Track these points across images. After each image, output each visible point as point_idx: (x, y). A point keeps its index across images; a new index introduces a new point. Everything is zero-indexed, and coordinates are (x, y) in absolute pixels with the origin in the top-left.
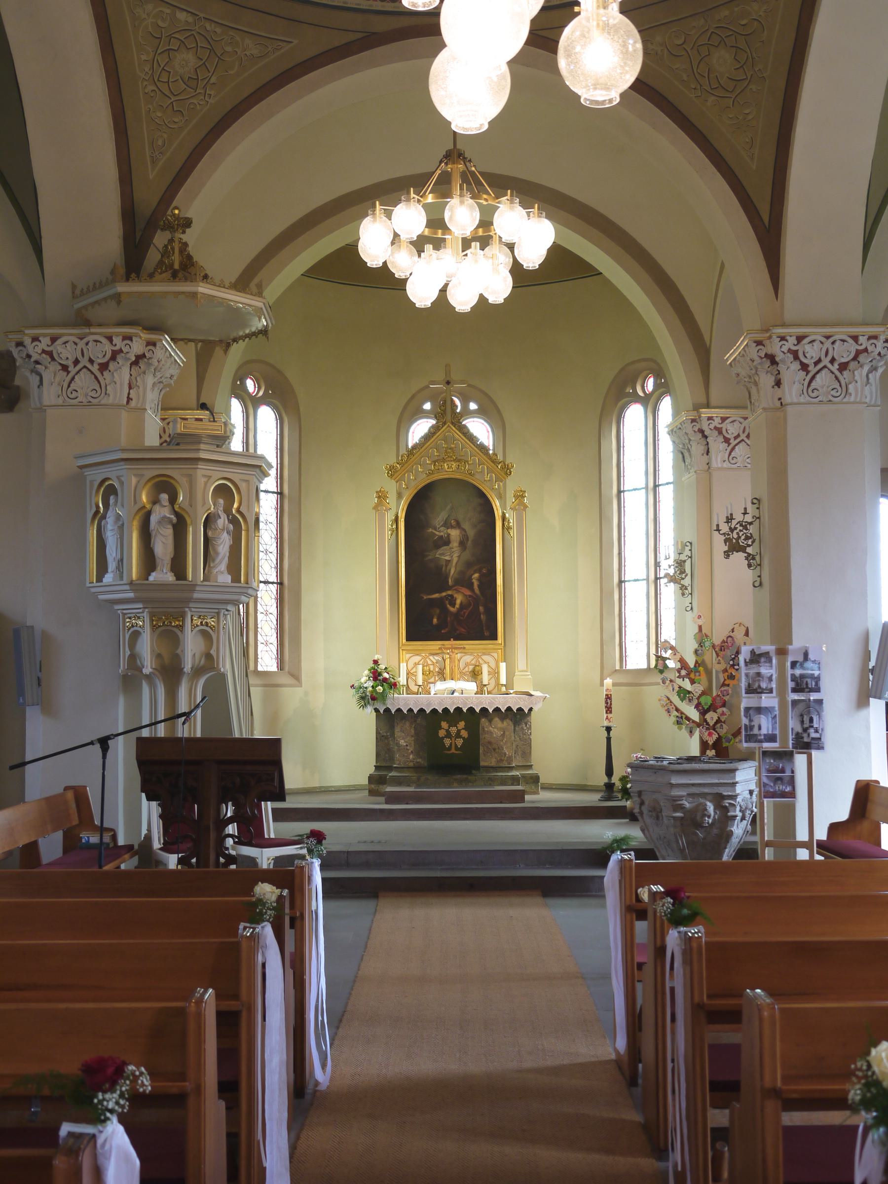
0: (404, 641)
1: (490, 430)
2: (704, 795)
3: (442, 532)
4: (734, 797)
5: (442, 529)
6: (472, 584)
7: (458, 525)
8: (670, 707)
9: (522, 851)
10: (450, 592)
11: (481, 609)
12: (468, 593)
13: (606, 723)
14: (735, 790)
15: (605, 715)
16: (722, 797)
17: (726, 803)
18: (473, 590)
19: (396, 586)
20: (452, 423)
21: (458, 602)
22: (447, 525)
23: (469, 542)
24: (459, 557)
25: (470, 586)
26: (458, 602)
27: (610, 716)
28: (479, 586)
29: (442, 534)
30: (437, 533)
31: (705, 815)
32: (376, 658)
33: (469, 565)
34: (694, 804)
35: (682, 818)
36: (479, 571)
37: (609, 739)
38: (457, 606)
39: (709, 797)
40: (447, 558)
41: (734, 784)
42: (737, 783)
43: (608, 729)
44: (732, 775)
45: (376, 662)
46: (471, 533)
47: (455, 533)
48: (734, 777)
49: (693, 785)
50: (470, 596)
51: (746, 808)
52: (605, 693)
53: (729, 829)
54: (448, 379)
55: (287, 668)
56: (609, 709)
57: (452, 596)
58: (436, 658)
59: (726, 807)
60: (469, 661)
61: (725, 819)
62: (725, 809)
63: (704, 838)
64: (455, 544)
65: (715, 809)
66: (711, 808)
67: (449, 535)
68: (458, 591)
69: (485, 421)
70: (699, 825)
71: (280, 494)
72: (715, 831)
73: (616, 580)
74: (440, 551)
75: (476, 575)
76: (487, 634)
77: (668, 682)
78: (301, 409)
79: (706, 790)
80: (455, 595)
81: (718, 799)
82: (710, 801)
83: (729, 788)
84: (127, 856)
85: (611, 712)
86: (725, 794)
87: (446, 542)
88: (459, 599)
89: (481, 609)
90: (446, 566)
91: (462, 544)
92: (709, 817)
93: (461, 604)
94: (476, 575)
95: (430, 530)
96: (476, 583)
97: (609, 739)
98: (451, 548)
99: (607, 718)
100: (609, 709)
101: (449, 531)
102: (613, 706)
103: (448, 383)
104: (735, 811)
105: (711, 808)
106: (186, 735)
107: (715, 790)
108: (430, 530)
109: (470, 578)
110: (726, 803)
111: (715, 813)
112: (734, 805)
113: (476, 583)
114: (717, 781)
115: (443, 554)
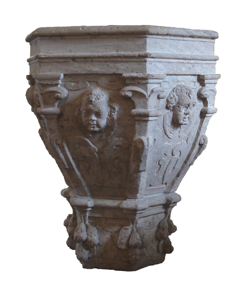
2: (93, 78)
4: (143, 81)
16: (124, 81)
31: (89, 112)
34: (78, 93)
39: (104, 81)
41: (142, 58)
44: (139, 42)
49: (74, 59)
53: (137, 137)
59: (129, 98)
62: (128, 102)
63: (100, 152)
65: (111, 101)
66: (101, 97)
70: (84, 129)
72: (116, 140)
79: (96, 68)
81: (116, 82)
82: (104, 88)
83: (134, 66)
84: (86, 261)
86: (125, 75)
92: (98, 114)
105: (101, 97)
106: (205, 82)
107: (110, 68)
110: (127, 91)
111: (112, 108)
112: (142, 96)
114: (114, 53)
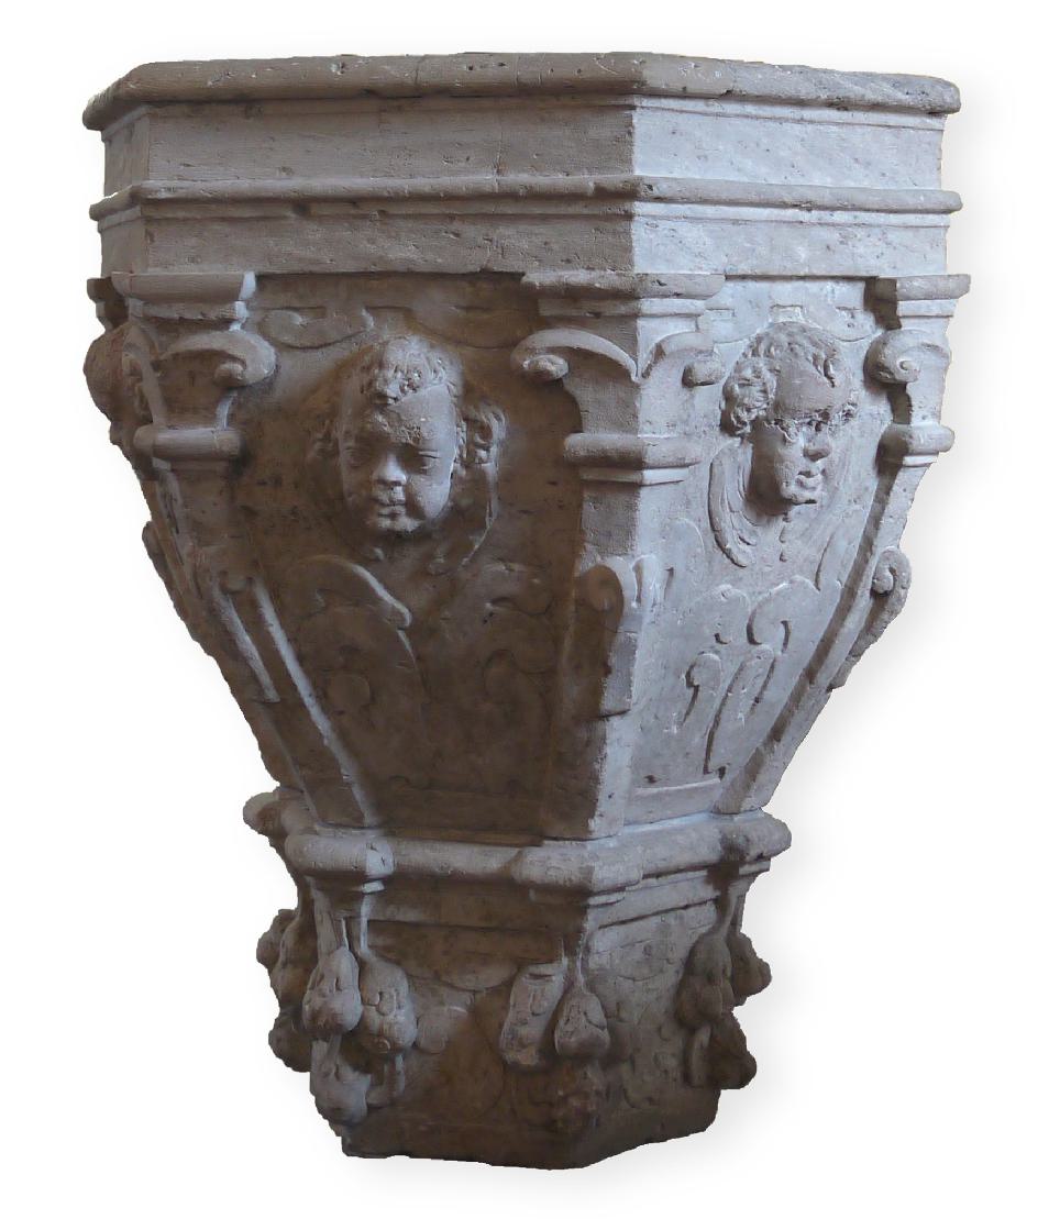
2: (392, 291)
4: (614, 305)
19: (754, 197)
31: (372, 447)
34: (322, 361)
35: (239, 463)
41: (614, 203)
42: (630, 193)
44: (601, 129)
49: (303, 205)
51: (780, 409)
53: (588, 561)
63: (422, 630)
65: (470, 397)
66: (424, 380)
70: (349, 522)
72: (495, 575)
79: (404, 249)
83: (580, 236)
92: (414, 458)
105: (424, 380)
107: (471, 248)
110: (547, 353)
112: (613, 372)
114: (487, 179)
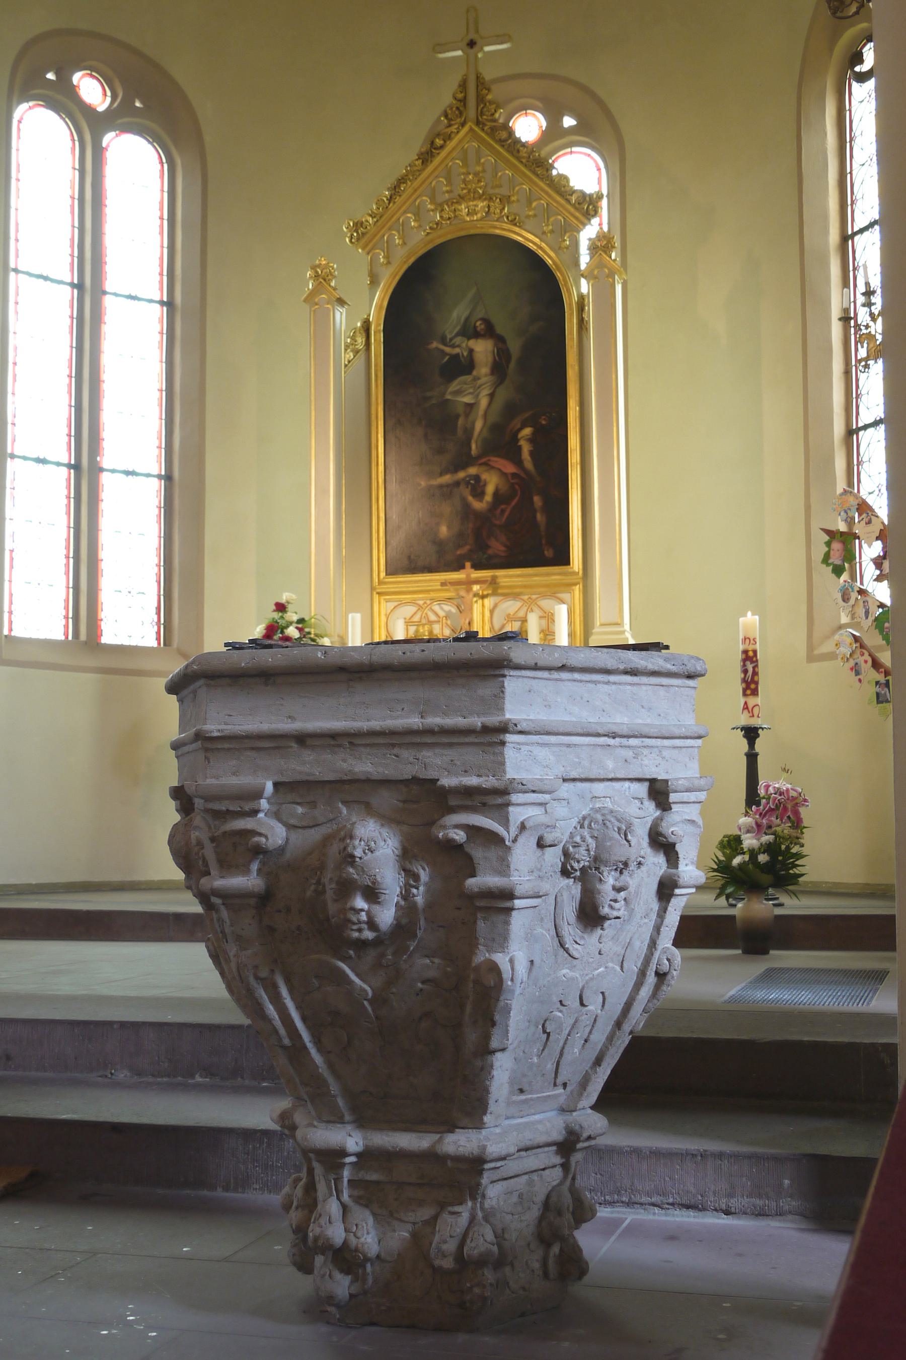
0: (383, 574)
1: (601, 164)
2: (357, 791)
3: (461, 347)
4: (495, 799)
5: (458, 340)
6: (520, 448)
7: (489, 331)
8: (861, 660)
9: (123, 1025)
10: (473, 471)
11: (537, 500)
12: (510, 468)
13: (744, 720)
14: (500, 765)
15: (742, 700)
17: (453, 828)
18: (519, 462)
20: (478, 123)
21: (490, 489)
22: (469, 332)
23: (513, 364)
24: (492, 396)
25: (513, 454)
26: (490, 489)
27: (752, 701)
28: (532, 454)
29: (457, 350)
30: (448, 350)
31: (346, 888)
32: (283, 600)
33: (510, 410)
34: (315, 835)
35: (264, 899)
36: (531, 422)
37: (752, 758)
38: (488, 498)
39: (386, 799)
40: (467, 399)
41: (494, 734)
43: (751, 734)
44: (485, 690)
45: (281, 607)
46: (515, 346)
47: (483, 349)
48: (497, 700)
49: (302, 739)
50: (514, 475)
51: (597, 861)
52: (741, 647)
53: (481, 956)
54: (472, 36)
55: (175, 643)
56: (750, 686)
57: (477, 478)
58: (447, 608)
60: (512, 611)
61: (465, 909)
62: (456, 859)
63: (379, 1000)
64: (483, 370)
65: (406, 856)
66: (378, 847)
67: (471, 351)
68: (488, 466)
69: (593, 148)
70: (334, 934)
71: (169, 304)
72: (424, 966)
73: (839, 428)
74: (454, 386)
75: (527, 431)
76: (549, 553)
77: (854, 595)
78: (207, 139)
79: (365, 765)
80: (485, 476)
81: (421, 806)
82: (388, 819)
83: (471, 756)
85: (755, 692)
86: (447, 781)
87: (462, 366)
88: (492, 483)
89: (537, 500)
90: (467, 415)
91: (499, 369)
92: (372, 894)
93: (496, 494)
94: (527, 431)
95: (435, 345)
96: (526, 448)
97: (752, 758)
98: (477, 379)
99: (746, 707)
100: (750, 686)
101: (472, 343)
102: (761, 678)
103: (472, 44)
104: (504, 868)
105: (378, 847)
108: (435, 345)
109: (515, 438)
110: (453, 828)
111: (411, 876)
112: (494, 839)
113: (526, 448)
114: (415, 721)
115: (458, 392)
